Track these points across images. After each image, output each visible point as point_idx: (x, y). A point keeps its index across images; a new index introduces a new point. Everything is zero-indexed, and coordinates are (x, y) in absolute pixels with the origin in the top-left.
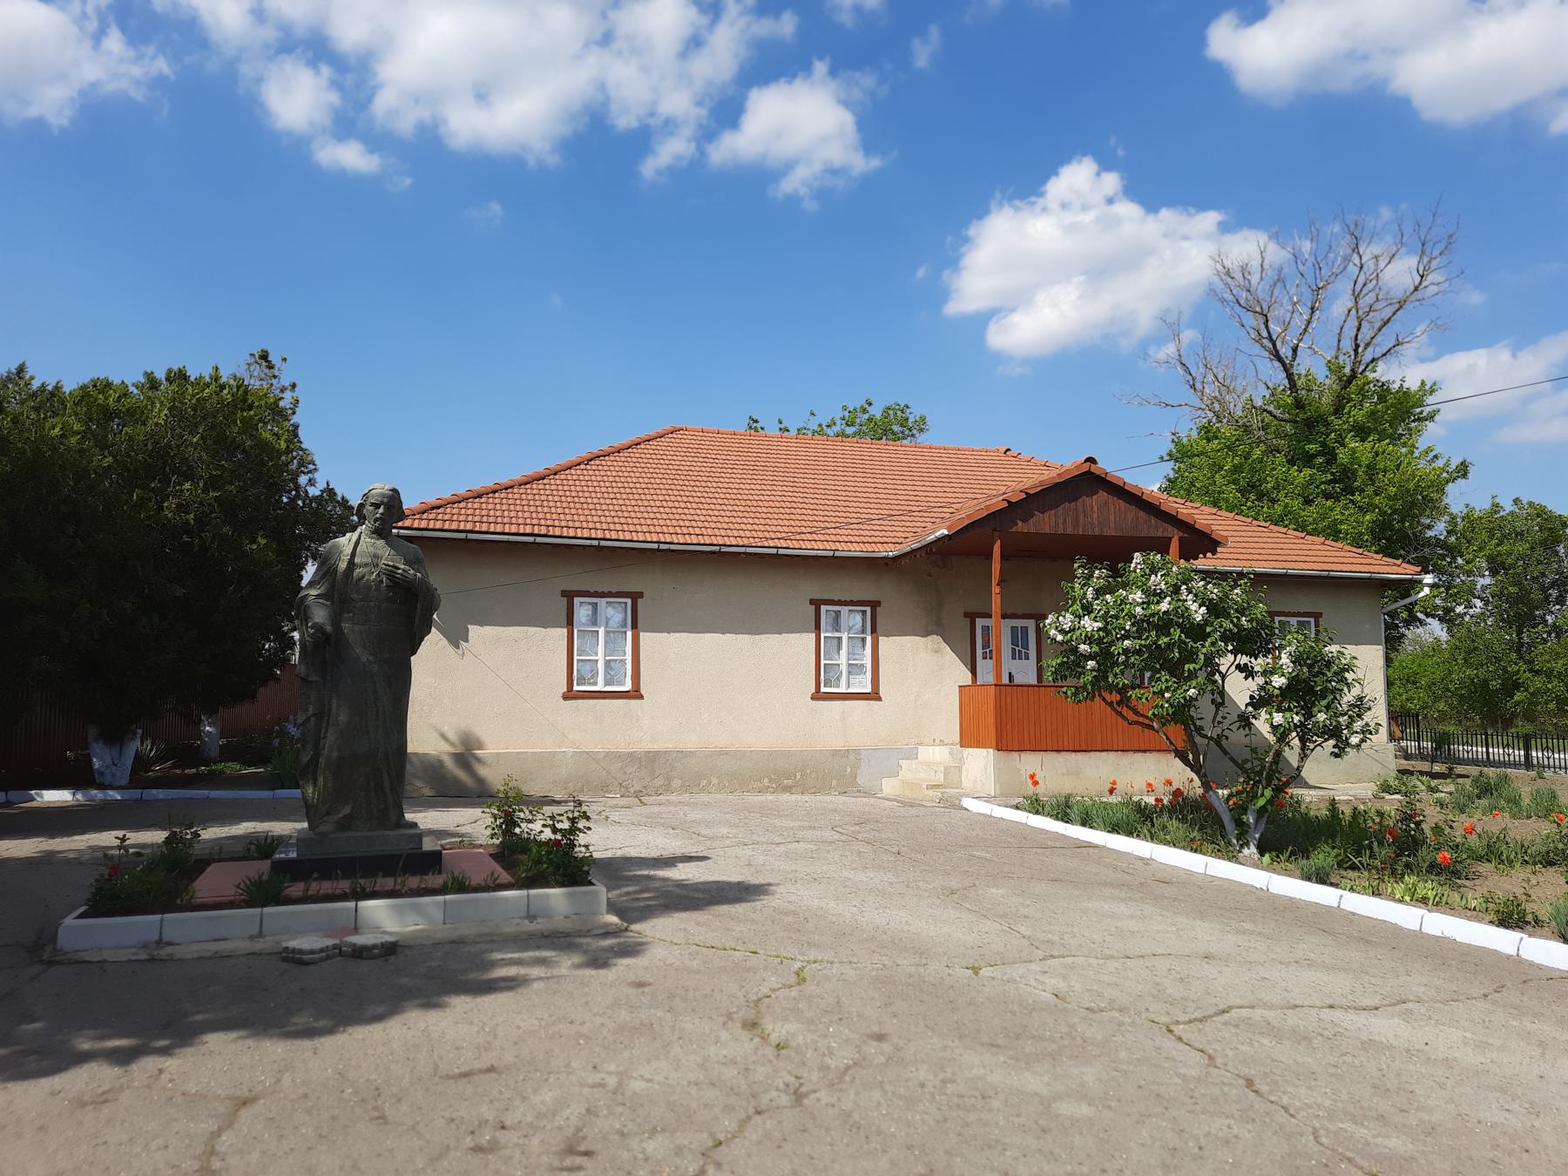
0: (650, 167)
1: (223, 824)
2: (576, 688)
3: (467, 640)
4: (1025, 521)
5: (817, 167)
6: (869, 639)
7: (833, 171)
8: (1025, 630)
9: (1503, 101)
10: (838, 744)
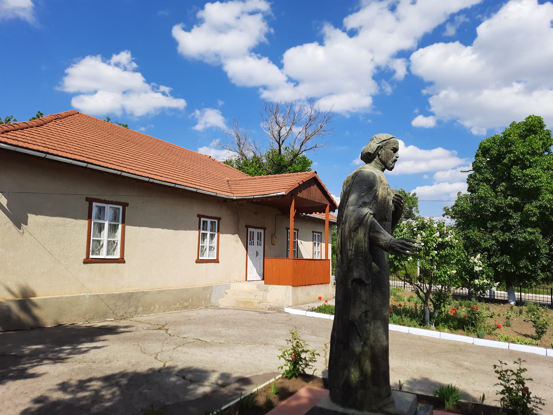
2: (91, 257)
3: (26, 224)
6: (216, 234)
8: (261, 233)
9: (252, 84)
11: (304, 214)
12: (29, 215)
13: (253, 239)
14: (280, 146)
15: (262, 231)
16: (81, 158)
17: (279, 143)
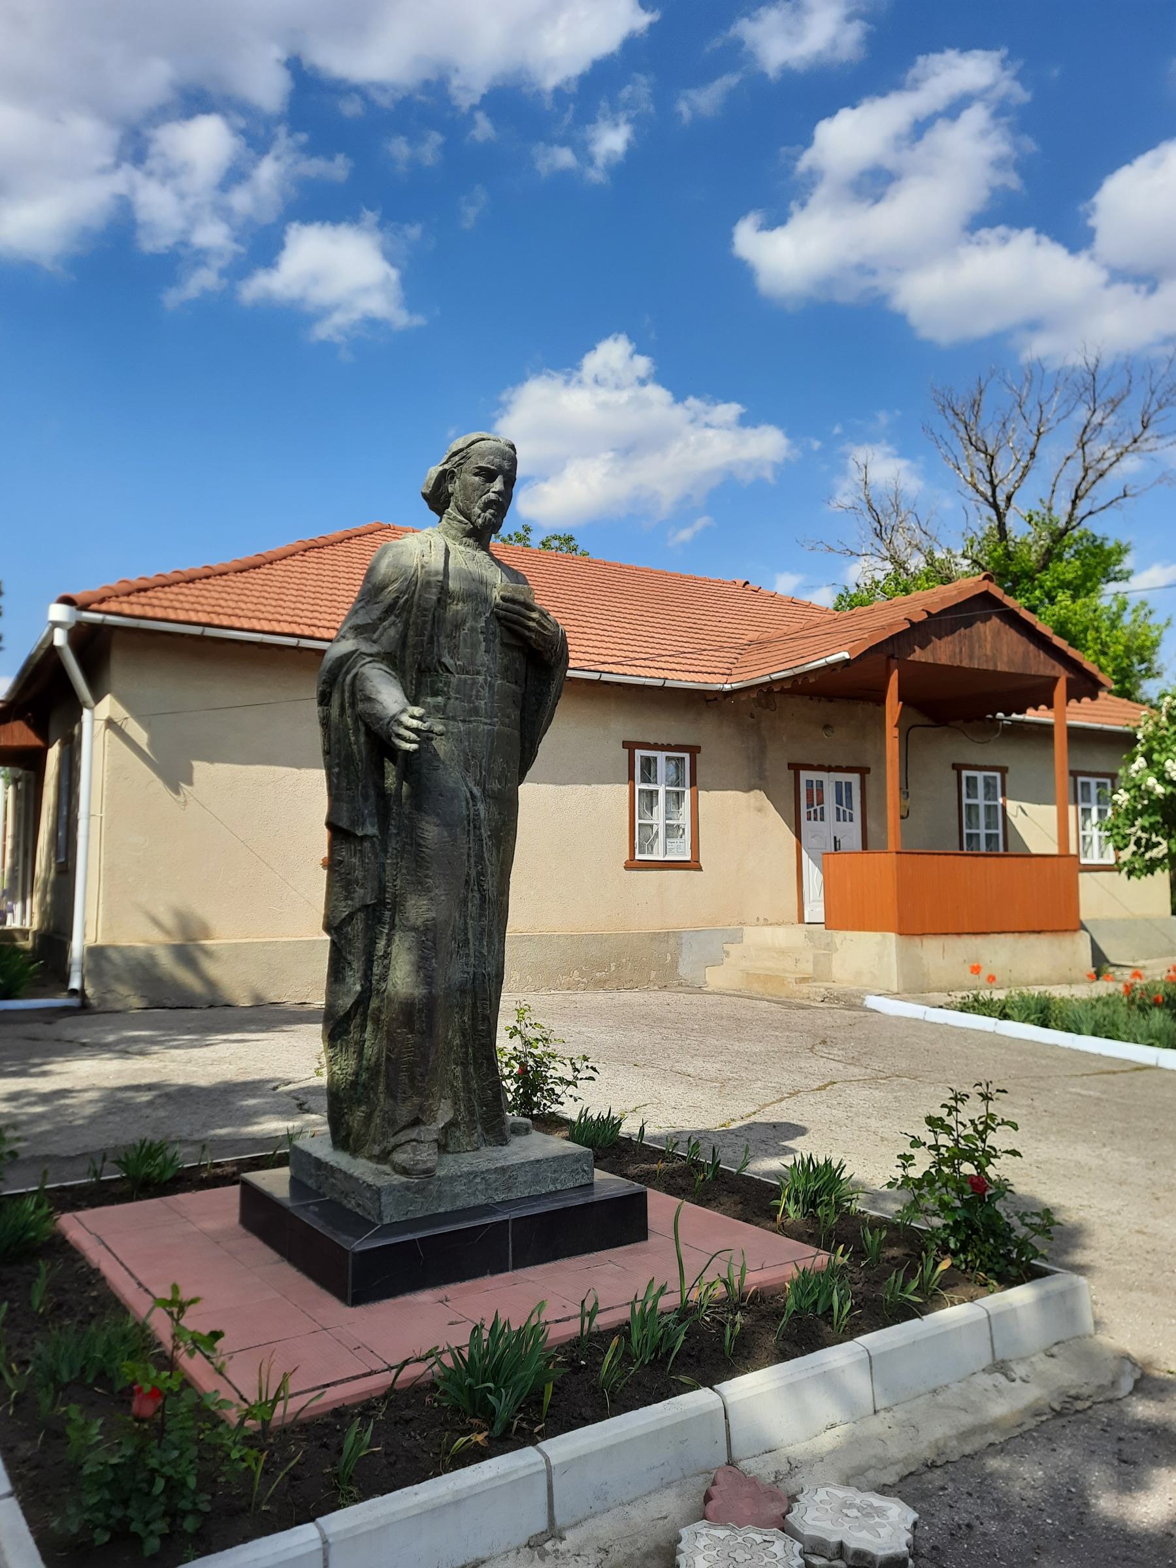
0: (172, 298)
1: (411, 1232)
3: (190, 783)
4: (922, 647)
5: (355, 316)
6: (688, 793)
7: (372, 323)
8: (849, 785)
9: (984, 326)
10: (654, 925)
11: (1000, 715)
12: (195, 764)
13: (820, 802)
14: (1000, 516)
15: (854, 778)
16: (287, 628)
17: (995, 506)
